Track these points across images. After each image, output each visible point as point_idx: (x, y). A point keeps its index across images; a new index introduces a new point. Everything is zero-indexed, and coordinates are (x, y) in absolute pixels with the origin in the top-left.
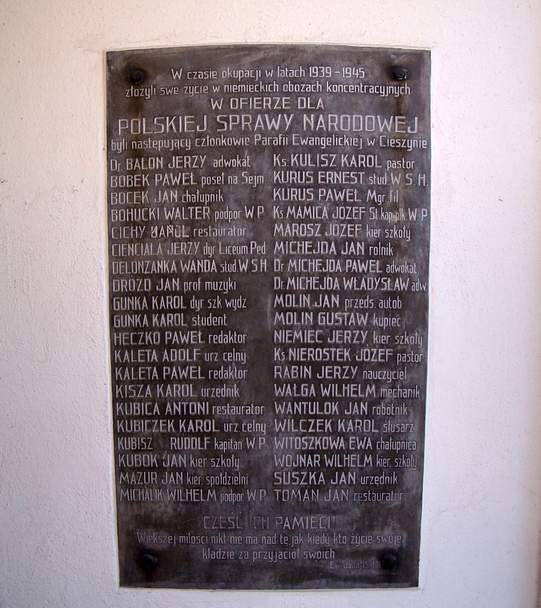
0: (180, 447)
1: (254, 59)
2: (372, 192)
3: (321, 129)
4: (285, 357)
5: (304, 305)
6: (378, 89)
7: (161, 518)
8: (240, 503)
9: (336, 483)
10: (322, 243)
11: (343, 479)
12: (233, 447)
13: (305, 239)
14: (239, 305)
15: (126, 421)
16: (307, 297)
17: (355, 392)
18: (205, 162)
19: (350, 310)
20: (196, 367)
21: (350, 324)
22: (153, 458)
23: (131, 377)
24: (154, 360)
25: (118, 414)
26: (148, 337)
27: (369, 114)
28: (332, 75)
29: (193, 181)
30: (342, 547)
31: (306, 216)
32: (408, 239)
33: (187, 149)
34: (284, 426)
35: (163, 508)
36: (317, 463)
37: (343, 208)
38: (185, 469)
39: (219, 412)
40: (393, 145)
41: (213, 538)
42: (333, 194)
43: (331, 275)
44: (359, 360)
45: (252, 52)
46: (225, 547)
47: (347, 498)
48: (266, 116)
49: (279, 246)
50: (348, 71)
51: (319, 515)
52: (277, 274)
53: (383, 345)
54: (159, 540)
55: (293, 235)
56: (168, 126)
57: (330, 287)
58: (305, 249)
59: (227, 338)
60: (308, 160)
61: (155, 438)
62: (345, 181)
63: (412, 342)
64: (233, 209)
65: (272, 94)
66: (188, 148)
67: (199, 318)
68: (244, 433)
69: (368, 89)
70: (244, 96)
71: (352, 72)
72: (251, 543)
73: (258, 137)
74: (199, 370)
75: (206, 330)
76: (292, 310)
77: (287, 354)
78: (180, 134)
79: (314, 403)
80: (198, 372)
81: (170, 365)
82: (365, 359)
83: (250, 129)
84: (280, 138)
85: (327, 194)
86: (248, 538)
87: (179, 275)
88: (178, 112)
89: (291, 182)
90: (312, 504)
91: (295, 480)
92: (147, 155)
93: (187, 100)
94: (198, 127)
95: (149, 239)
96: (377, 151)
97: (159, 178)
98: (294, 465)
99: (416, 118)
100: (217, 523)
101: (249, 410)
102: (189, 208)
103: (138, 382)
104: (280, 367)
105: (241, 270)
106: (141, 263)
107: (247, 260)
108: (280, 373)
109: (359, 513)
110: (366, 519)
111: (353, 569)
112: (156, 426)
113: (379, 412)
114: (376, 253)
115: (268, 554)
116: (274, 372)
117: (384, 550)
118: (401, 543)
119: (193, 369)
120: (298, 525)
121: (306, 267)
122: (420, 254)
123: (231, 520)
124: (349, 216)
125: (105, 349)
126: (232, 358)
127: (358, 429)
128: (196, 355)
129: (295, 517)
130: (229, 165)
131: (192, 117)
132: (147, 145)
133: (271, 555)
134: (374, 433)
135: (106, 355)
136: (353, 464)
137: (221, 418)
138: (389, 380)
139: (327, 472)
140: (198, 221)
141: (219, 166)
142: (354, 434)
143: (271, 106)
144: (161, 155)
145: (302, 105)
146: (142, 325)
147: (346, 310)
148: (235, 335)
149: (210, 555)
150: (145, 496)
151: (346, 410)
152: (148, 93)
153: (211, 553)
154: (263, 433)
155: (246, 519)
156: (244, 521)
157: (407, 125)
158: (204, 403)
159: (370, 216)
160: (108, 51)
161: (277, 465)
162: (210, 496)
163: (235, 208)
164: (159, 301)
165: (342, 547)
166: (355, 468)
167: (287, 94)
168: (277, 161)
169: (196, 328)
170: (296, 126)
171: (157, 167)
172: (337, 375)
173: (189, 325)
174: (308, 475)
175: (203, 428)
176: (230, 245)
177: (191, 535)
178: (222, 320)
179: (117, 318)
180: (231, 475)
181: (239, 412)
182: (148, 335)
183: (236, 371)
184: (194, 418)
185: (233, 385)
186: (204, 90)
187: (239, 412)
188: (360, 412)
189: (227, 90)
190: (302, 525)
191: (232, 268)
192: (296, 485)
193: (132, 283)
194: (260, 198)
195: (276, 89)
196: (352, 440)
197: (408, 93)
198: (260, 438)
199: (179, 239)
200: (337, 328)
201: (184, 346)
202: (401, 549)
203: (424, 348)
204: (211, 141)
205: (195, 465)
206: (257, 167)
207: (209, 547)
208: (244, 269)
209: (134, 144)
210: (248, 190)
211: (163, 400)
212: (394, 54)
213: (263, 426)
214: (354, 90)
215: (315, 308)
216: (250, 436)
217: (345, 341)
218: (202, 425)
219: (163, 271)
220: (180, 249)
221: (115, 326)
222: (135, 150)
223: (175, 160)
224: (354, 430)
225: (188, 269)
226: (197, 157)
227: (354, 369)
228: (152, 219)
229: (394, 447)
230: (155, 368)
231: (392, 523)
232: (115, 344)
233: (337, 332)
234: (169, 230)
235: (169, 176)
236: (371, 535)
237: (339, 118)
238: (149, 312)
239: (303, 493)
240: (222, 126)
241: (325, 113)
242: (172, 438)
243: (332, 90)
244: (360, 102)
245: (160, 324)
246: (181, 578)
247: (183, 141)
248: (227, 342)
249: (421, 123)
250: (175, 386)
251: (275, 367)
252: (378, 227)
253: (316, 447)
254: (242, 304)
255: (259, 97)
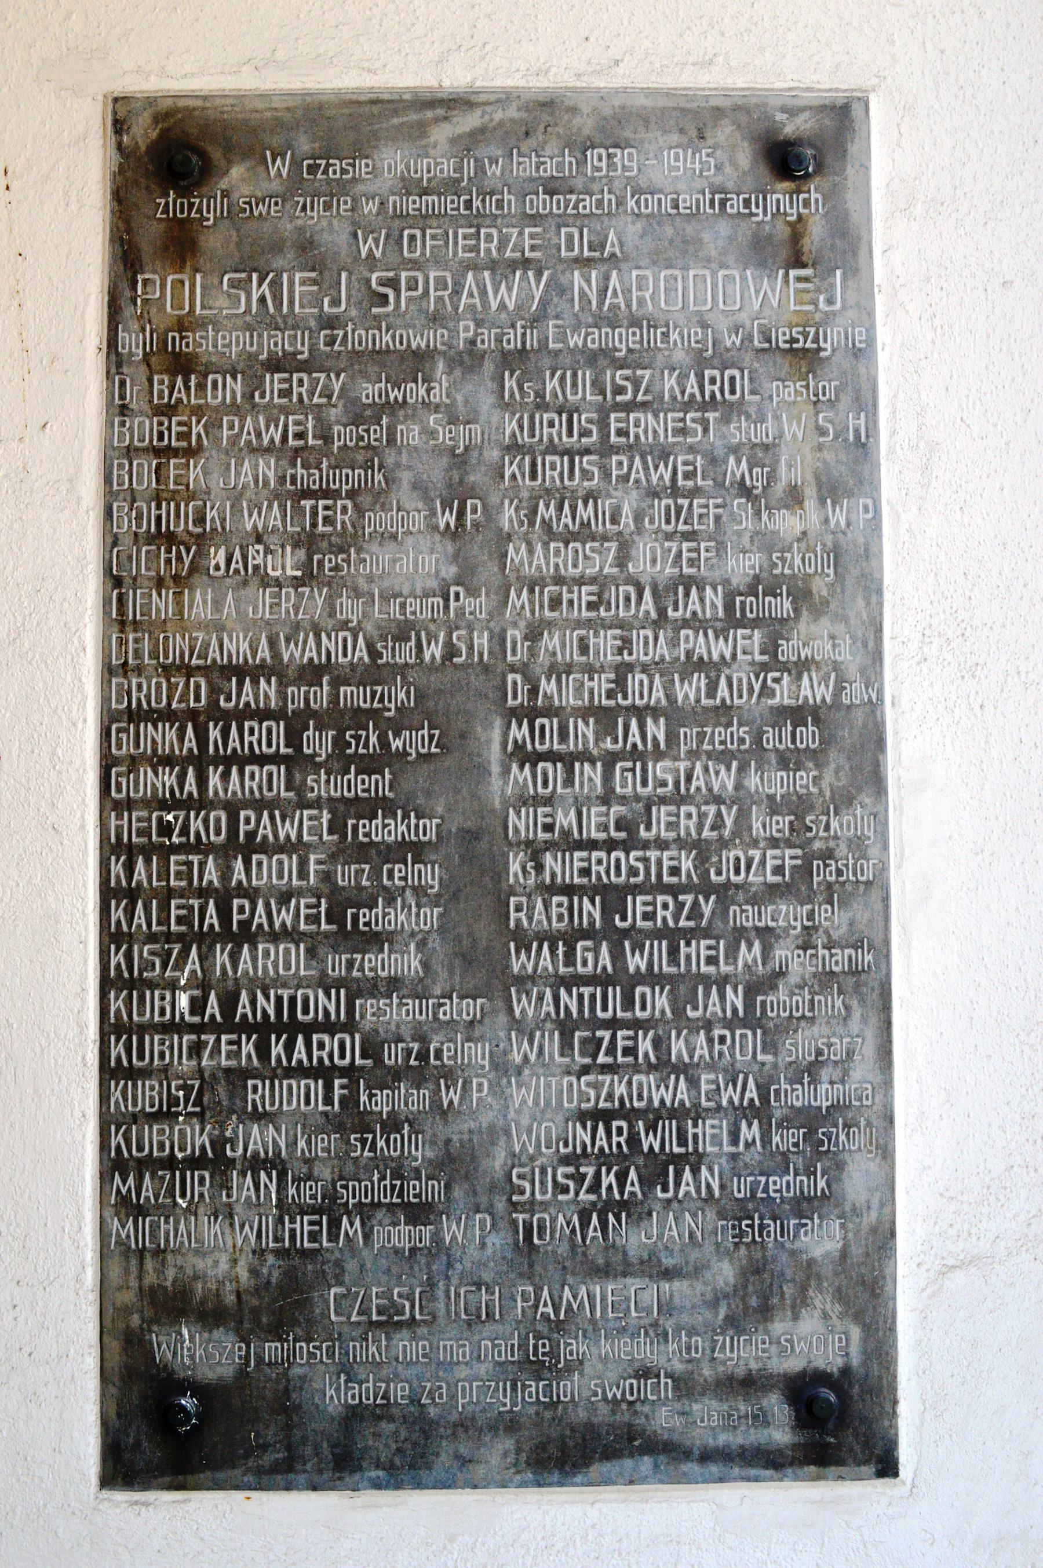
0: (272, 1104)
1: (459, 130)
2: (738, 462)
3: (614, 307)
4: (537, 875)
5: (580, 746)
6: (747, 203)
7: (218, 1295)
8: (426, 1252)
9: (670, 1194)
10: (621, 588)
11: (688, 1184)
12: (406, 1104)
13: (581, 581)
14: (423, 746)
15: (134, 1038)
16: (587, 724)
17: (712, 961)
18: (342, 389)
19: (693, 755)
20: (314, 900)
21: (692, 790)
22: (201, 1134)
23: (149, 925)
24: (211, 882)
25: (112, 1021)
26: (196, 825)
27: (727, 267)
28: (639, 170)
29: (314, 437)
30: (690, 1367)
31: (582, 524)
32: (828, 575)
33: (299, 357)
34: (535, 1049)
35: (224, 1266)
36: (619, 1145)
37: (670, 501)
38: (282, 1161)
39: (373, 1014)
40: (786, 342)
41: (354, 1347)
42: (646, 468)
43: (645, 669)
44: (719, 878)
45: (455, 113)
46: (385, 1372)
47: (699, 1234)
48: (487, 274)
49: (519, 599)
50: (677, 159)
51: (629, 1281)
52: (513, 669)
53: (777, 840)
54: (209, 1356)
55: (552, 570)
56: (255, 297)
57: (642, 697)
58: (580, 605)
59: (393, 827)
60: (584, 386)
61: (206, 1081)
62: (673, 436)
63: (849, 830)
64: (408, 507)
65: (499, 220)
66: (302, 353)
67: (323, 777)
68: (436, 1067)
69: (723, 203)
70: (435, 224)
71: (685, 160)
72: (452, 1357)
73: (467, 329)
74: (323, 909)
75: (341, 807)
76: (551, 756)
77: (539, 868)
78: (284, 317)
79: (610, 989)
80: (319, 913)
81: (251, 894)
82: (732, 877)
83: (449, 308)
84: (520, 331)
85: (630, 468)
86: (445, 1347)
87: (274, 669)
88: (281, 262)
89: (545, 439)
90: (611, 1251)
91: (565, 1190)
92: (202, 368)
93: (301, 230)
94: (326, 301)
95: (205, 578)
96: (748, 358)
97: (231, 427)
98: (562, 1150)
99: (838, 273)
100: (364, 1306)
101: (448, 1008)
102: (303, 502)
103: (169, 937)
104: (524, 899)
105: (427, 658)
106: (184, 639)
107: (442, 634)
108: (522, 915)
109: (731, 1273)
110: (750, 1288)
111: (725, 1429)
112: (212, 1053)
113: (772, 1011)
114: (751, 612)
115: (497, 1388)
116: (508, 912)
117: (803, 1374)
118: (847, 1354)
119: (308, 907)
120: (575, 1307)
121: (584, 649)
122: (859, 613)
123: (400, 1296)
124: (685, 523)
125: (85, 852)
126: (405, 879)
127: (721, 1054)
128: (316, 871)
129: (566, 1288)
130: (400, 399)
131: (313, 275)
132: (204, 342)
133: (505, 1390)
134: (763, 1064)
135: (87, 867)
136: (712, 1144)
137: (376, 1031)
138: (795, 928)
139: (645, 1166)
140: (323, 535)
141: (377, 399)
142: (712, 1067)
143: (499, 249)
144: (239, 369)
145: (570, 248)
146: (182, 793)
147: (682, 755)
148: (413, 821)
149: (346, 1394)
150: (176, 1236)
151: (689, 1007)
152: (209, 212)
153: (347, 1388)
154: (483, 1067)
155: (440, 1294)
156: (433, 1299)
157: (818, 291)
158: (333, 991)
159: (734, 520)
160: (116, 95)
161: (517, 1150)
162: (347, 1234)
163: (413, 506)
164: (225, 734)
165: (690, 1367)
166: (719, 1155)
167: (535, 219)
168: (511, 388)
169: (317, 804)
170: (555, 299)
171: (228, 401)
172: (664, 919)
173: (298, 794)
174: (598, 1174)
175: (331, 1056)
176: (400, 595)
177: (295, 1341)
178: (381, 784)
179: (118, 775)
180: (401, 1177)
181: (421, 1013)
182: (196, 818)
183: (414, 910)
184: (308, 1030)
185: (407, 945)
186: (342, 207)
187: (421, 1013)
188: (724, 1011)
189: (395, 207)
190: (584, 1308)
191: (405, 654)
192: (567, 1203)
193: (159, 686)
194: (472, 479)
195: (509, 208)
196: (708, 1082)
197: (817, 210)
198: (475, 1081)
199: (277, 580)
200: (663, 801)
201: (286, 847)
202: (846, 1371)
203: (878, 845)
204: (358, 337)
205: (310, 1151)
206: (466, 402)
207: (342, 1371)
208: (433, 657)
209: (174, 338)
210: (445, 461)
211: (230, 983)
212: (784, 109)
213: (483, 1048)
214: (690, 208)
215: (606, 751)
216: (448, 1075)
217: (682, 833)
218: (327, 1049)
219: (238, 658)
220: (279, 604)
221: (113, 794)
222: (176, 356)
223: (272, 381)
224: (712, 1058)
225: (297, 655)
226: (323, 376)
227: (707, 901)
228: (212, 529)
229: (816, 1100)
230: (211, 902)
231: (821, 1300)
232: (113, 840)
233: (663, 808)
234: (254, 558)
235: (256, 421)
236: (767, 1332)
237: (656, 279)
238: (200, 762)
239: (585, 1223)
240: (384, 300)
241: (624, 266)
242: (250, 1083)
243: (639, 208)
244: (706, 236)
245: (226, 790)
246: (269, 1458)
247: (289, 336)
248: (393, 838)
249: (850, 283)
250: (260, 947)
251: (512, 899)
252: (755, 549)
253: (617, 1103)
254: (430, 742)
255: (471, 227)
